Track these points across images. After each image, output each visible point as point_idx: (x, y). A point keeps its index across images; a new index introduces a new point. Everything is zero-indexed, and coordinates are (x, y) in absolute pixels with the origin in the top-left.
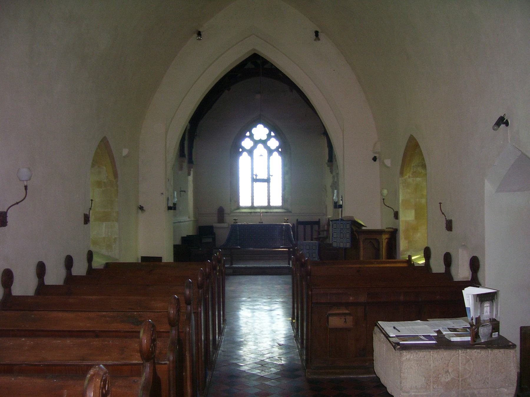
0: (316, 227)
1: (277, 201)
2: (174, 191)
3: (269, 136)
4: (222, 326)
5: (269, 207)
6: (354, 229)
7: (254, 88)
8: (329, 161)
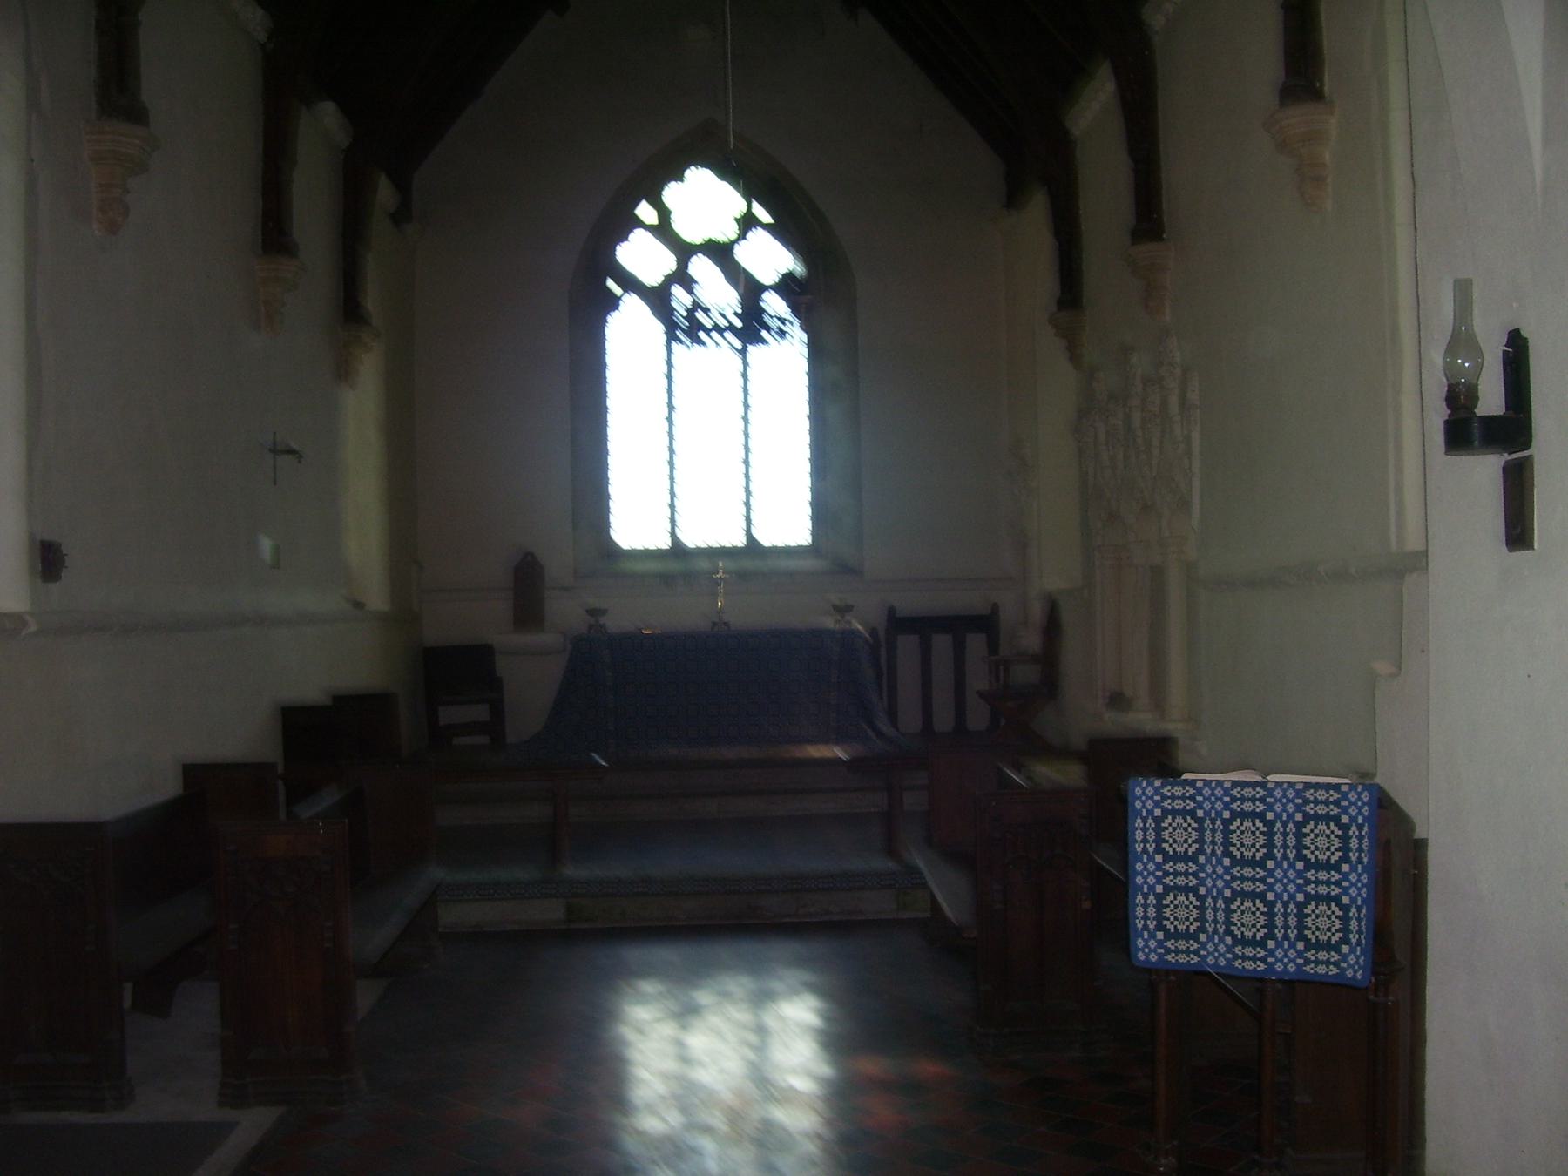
0: (976, 643)
1: (787, 522)
3: (747, 223)
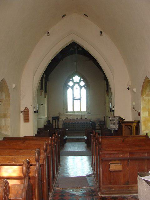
1: (84, 109)
2: (37, 104)
3: (80, 81)
4: (58, 168)
5: (80, 112)
6: (120, 121)
7: (73, 58)
8: (107, 91)
